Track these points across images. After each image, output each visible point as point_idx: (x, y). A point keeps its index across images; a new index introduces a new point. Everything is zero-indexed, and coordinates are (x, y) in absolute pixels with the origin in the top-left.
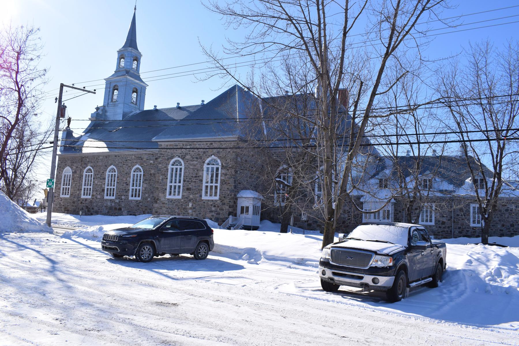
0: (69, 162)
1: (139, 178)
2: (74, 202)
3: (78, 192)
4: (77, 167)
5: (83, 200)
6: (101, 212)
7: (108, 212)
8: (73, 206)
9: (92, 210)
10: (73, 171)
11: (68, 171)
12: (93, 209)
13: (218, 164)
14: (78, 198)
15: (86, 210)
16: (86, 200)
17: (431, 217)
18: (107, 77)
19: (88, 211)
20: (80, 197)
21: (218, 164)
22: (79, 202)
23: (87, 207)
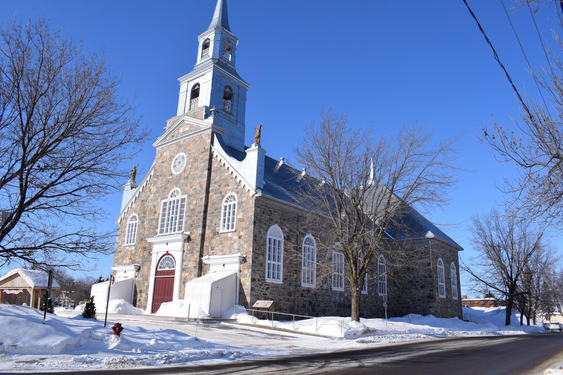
0: (276, 216)
1: (171, 211)
2: (290, 294)
3: (295, 276)
4: (291, 230)
5: (304, 291)
6: (329, 311)
7: (338, 311)
8: (288, 300)
9: (317, 309)
10: (286, 235)
11: (275, 232)
12: (319, 306)
13: (280, 237)
14: (296, 286)
15: (310, 307)
16: (308, 290)
17: (164, 210)
18: (1, 299)
19: (313, 309)
20: (300, 285)
21: (280, 237)
22: (298, 294)
23: (310, 303)
